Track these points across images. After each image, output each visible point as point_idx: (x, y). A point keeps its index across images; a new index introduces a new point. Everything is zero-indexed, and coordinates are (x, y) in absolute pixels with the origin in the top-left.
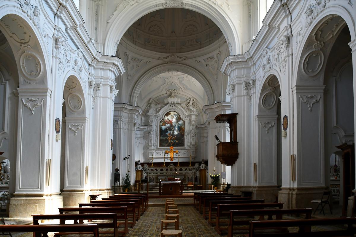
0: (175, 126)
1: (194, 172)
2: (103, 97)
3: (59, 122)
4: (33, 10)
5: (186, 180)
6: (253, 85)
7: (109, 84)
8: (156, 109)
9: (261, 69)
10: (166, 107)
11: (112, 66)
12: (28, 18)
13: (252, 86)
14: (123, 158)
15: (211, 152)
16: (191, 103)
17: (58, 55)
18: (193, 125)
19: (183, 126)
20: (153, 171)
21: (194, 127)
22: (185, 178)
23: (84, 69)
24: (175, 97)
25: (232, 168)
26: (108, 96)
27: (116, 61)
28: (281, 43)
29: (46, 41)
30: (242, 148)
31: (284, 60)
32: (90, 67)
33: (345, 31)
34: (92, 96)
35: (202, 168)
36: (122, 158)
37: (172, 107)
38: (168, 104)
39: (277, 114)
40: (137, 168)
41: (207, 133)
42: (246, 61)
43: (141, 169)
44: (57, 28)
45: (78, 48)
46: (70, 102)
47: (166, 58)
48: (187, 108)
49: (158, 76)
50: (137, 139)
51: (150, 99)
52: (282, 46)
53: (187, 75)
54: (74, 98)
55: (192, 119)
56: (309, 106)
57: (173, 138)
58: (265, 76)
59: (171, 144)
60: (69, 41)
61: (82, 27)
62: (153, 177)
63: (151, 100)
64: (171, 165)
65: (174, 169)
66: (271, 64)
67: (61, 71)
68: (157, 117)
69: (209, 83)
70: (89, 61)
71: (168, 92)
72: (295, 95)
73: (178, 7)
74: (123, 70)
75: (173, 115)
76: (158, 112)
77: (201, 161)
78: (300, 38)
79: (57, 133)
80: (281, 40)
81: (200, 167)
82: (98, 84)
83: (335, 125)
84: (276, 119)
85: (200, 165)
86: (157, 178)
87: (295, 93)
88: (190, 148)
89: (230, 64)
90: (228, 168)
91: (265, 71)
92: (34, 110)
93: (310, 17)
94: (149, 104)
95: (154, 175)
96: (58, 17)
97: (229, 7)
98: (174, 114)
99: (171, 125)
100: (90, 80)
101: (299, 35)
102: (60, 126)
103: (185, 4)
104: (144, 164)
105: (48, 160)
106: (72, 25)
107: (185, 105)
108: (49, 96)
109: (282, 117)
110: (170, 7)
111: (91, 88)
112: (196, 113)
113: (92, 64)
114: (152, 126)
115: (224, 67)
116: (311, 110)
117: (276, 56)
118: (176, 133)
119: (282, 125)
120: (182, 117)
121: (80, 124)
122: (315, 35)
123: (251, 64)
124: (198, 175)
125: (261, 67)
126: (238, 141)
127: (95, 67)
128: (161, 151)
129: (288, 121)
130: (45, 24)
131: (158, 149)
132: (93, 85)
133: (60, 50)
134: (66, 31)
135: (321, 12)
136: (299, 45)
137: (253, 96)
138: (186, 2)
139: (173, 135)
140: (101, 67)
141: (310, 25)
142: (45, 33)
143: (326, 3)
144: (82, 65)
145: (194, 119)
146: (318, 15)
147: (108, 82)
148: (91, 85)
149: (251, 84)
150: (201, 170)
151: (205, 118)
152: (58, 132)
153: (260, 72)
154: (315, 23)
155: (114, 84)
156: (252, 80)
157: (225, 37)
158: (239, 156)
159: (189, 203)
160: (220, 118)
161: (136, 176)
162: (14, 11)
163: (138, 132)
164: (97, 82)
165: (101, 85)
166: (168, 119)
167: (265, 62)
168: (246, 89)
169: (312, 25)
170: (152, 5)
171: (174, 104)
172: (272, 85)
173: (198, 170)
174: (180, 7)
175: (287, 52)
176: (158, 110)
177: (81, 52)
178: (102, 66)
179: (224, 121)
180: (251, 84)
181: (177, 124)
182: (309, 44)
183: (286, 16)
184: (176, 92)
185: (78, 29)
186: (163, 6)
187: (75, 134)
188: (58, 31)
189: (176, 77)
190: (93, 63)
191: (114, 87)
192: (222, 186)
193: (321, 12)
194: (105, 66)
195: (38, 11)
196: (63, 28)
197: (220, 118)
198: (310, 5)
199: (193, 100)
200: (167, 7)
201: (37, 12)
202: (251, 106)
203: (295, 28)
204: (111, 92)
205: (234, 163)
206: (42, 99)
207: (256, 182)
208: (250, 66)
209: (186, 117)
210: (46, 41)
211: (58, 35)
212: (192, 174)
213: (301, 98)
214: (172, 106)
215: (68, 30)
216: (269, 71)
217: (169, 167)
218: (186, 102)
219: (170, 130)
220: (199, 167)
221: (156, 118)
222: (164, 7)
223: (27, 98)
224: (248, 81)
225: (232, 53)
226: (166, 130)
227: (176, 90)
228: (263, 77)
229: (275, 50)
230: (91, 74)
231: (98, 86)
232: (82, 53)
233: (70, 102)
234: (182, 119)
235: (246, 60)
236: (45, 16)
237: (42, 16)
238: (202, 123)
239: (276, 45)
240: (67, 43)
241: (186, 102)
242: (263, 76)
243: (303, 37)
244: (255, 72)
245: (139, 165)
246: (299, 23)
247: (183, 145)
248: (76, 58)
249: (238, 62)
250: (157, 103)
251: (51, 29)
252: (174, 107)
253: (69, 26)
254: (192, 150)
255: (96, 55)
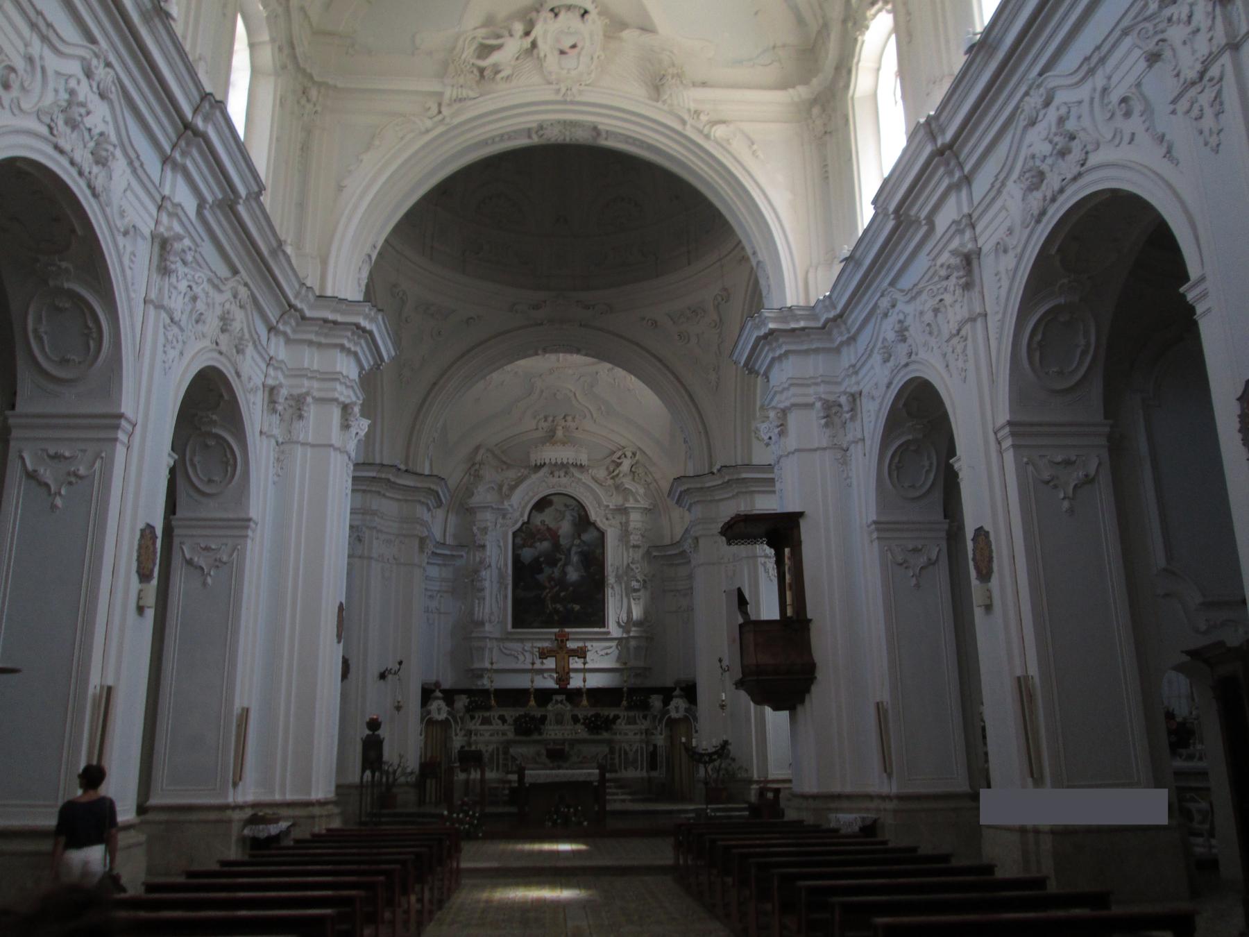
0: (569, 550)
1: (647, 731)
2: (313, 446)
3: (154, 537)
4: (91, 144)
5: (617, 761)
6: (852, 410)
7: (336, 400)
8: (500, 487)
9: (877, 358)
10: (534, 477)
11: (349, 334)
12: (74, 172)
13: (848, 416)
14: (376, 674)
15: (712, 653)
16: (626, 465)
17: (166, 296)
18: (634, 546)
19: (598, 551)
20: (491, 724)
21: (641, 552)
22: (612, 751)
23: (250, 344)
24: (567, 441)
25: (793, 719)
26: (333, 442)
27: (366, 317)
28: (943, 273)
29: (129, 249)
30: (828, 642)
31: (958, 333)
32: (272, 334)
33: (1160, 241)
34: (273, 442)
35: (674, 715)
36: (374, 669)
37: (555, 480)
38: (542, 466)
39: (946, 517)
40: (429, 712)
41: (690, 577)
42: (824, 327)
43: (443, 716)
44: (168, 205)
45: (235, 272)
46: (191, 460)
47: (536, 307)
48: (610, 482)
49: (508, 368)
50: (431, 597)
51: (478, 448)
52: (945, 283)
53: (609, 366)
54: (207, 446)
55: (632, 525)
56: (1062, 496)
57: (562, 594)
58: (895, 382)
59: (556, 618)
60: (208, 249)
61: (254, 205)
62: (490, 748)
63: (482, 451)
64: (557, 702)
65: (568, 716)
66: (910, 341)
67: (173, 354)
68: (504, 517)
69: (690, 396)
70: (270, 315)
71: (543, 424)
72: (1009, 456)
73: (581, 141)
74: (387, 350)
75: (563, 509)
76: (508, 496)
77: (669, 683)
78: (1008, 261)
79: (141, 581)
80: (942, 266)
81: (668, 712)
82: (299, 396)
83: (1162, 562)
84: (943, 534)
85: (666, 702)
86: (506, 752)
87: (1007, 449)
88: (628, 632)
89: (765, 337)
90: (776, 720)
91: (891, 364)
92: (63, 492)
93: (1038, 195)
94: (474, 464)
95: (494, 738)
96: (176, 166)
97: (755, 147)
98: (566, 506)
99: (556, 546)
100: (270, 382)
101: (1005, 251)
102: (155, 552)
103: (604, 135)
104: (456, 697)
105: (102, 687)
106: (220, 196)
107: (606, 473)
108: (123, 443)
109: (969, 534)
110: (553, 140)
111: (274, 411)
112: (644, 504)
113: (281, 327)
114: (484, 546)
115: (743, 349)
116: (1071, 511)
117: (929, 317)
118: (573, 575)
119: (971, 564)
120: (593, 516)
121: (84, 451)
122: (1059, 250)
123: (839, 339)
124: (660, 740)
125: (876, 351)
126: (809, 616)
127: (292, 336)
128: (519, 645)
129: (993, 547)
130: (129, 193)
131: (507, 638)
132: (281, 400)
133: (173, 279)
134: (199, 213)
135: (1075, 179)
136: (1005, 283)
137: (856, 452)
138: (608, 128)
139: (562, 582)
140: (313, 337)
141: (1038, 221)
142: (126, 220)
143: (1087, 153)
144: (246, 331)
145: (639, 525)
146: (1062, 191)
147: (335, 390)
148: (272, 402)
149: (846, 408)
150: (672, 723)
151: (677, 522)
152: (144, 576)
153: (872, 367)
154: (1054, 214)
155: (354, 399)
156: (845, 393)
157: (740, 242)
158: (819, 675)
159: (636, 863)
160: (742, 529)
161: (426, 743)
162: (32, 148)
163: (433, 571)
164: (296, 392)
165: (309, 400)
166: (543, 522)
167: (891, 336)
168: (827, 425)
169: (1045, 220)
170: (495, 133)
171: (564, 467)
172: (919, 418)
173: (660, 721)
174: (590, 142)
175: (965, 307)
176: (505, 489)
177: (246, 285)
178: (317, 334)
179: (750, 538)
180: (846, 408)
181: (577, 542)
182: (1041, 279)
183: (954, 187)
184: (570, 423)
185: (241, 209)
186: (530, 137)
187: (205, 580)
188: (170, 215)
189: (570, 372)
190: (285, 323)
191: (357, 409)
192: (755, 786)
193: (1075, 179)
194: (326, 335)
195: (111, 148)
196: (190, 205)
197: (742, 529)
198: (1033, 157)
199: (634, 454)
200: (543, 141)
201: (107, 150)
202: (850, 486)
203: (986, 227)
204: (346, 426)
205: (802, 701)
206: (234, 549)
207: (890, 776)
208: (837, 342)
209: (610, 516)
210: (129, 249)
211: (170, 228)
212: (638, 737)
213: (1030, 468)
214: (556, 474)
215: (207, 213)
216: (907, 365)
217: (550, 707)
218: (609, 460)
219: (553, 562)
220: (665, 712)
221: (500, 520)
222: (535, 140)
223: (42, 450)
224: (832, 398)
225: (773, 302)
226: (536, 567)
227: (569, 418)
228: (888, 387)
229: (924, 296)
230: (273, 362)
231: (298, 403)
232: (249, 289)
233: (191, 460)
234: (594, 524)
235: (820, 325)
236: (131, 163)
237: (119, 165)
238: (667, 541)
239: (927, 277)
240: (198, 256)
241: (609, 460)
242: (886, 381)
243: (1020, 258)
244: (858, 366)
245: (437, 698)
246: (1000, 211)
247: (601, 622)
248: (227, 306)
249: (793, 330)
250: (505, 463)
251: (146, 208)
252: (564, 480)
253: (210, 199)
254: (633, 643)
255: (297, 295)
